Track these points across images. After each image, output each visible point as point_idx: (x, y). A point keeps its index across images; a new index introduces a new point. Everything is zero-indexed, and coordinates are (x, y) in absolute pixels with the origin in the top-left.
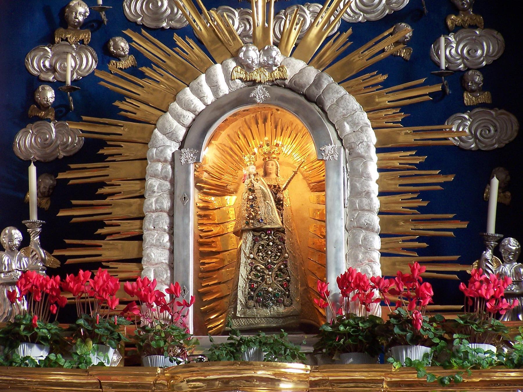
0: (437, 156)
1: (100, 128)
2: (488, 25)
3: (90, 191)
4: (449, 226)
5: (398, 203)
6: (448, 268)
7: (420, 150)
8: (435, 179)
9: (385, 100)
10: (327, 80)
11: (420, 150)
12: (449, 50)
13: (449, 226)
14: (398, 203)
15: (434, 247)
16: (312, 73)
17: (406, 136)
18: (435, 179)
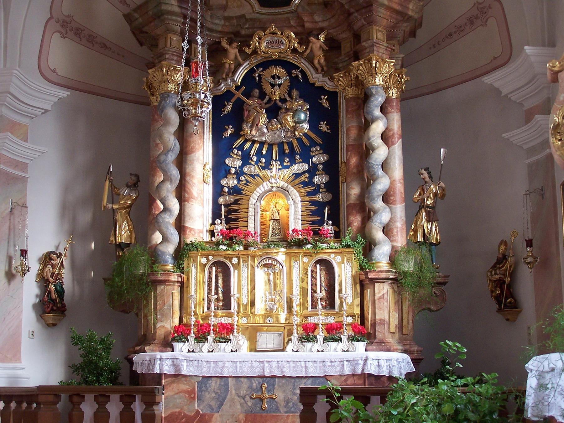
0: (314, 203)
2: (326, 174)
3: (236, 211)
4: (316, 218)
5: (305, 213)
6: (316, 228)
7: (310, 202)
8: (313, 208)
9: (302, 191)
10: (290, 186)
11: (310, 202)
12: (317, 180)
13: (316, 218)
14: (305, 213)
15: (313, 223)
16: (286, 184)
17: (307, 199)
18: (313, 208)
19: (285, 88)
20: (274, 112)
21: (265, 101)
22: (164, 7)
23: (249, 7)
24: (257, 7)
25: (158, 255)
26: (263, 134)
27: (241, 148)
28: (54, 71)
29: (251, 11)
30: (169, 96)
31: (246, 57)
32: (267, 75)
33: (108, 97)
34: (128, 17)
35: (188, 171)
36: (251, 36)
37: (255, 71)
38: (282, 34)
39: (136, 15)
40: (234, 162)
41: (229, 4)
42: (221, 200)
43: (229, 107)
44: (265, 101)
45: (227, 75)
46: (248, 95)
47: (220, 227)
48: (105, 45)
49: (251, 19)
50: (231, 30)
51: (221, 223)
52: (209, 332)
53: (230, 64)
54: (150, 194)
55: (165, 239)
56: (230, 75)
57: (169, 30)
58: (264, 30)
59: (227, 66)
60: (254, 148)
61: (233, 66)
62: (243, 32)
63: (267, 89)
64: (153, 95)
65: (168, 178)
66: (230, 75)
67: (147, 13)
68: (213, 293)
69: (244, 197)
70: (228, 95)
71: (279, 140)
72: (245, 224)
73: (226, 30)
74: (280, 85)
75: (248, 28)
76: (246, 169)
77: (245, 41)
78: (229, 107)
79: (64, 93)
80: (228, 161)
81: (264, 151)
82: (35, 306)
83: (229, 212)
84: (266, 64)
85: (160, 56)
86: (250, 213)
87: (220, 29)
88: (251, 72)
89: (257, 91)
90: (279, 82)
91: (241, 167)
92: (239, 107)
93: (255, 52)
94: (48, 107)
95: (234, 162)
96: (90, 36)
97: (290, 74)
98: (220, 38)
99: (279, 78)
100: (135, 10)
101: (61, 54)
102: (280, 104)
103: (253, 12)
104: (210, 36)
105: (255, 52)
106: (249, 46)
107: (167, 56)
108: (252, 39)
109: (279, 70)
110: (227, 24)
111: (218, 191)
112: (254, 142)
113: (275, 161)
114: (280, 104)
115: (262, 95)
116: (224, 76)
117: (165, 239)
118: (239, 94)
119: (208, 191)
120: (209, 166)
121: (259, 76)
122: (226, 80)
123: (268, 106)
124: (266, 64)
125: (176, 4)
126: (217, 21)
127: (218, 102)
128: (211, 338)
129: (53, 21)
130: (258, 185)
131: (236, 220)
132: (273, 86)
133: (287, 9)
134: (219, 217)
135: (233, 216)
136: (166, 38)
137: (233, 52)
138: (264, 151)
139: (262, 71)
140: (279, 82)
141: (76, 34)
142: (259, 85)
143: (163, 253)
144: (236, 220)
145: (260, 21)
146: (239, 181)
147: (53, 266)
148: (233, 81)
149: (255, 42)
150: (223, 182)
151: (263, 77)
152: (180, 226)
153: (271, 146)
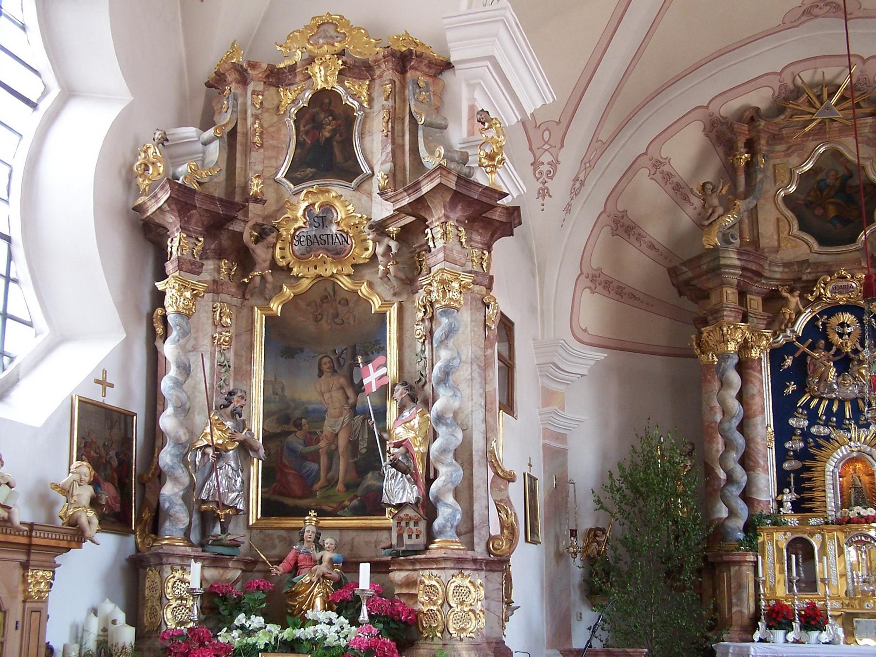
1: (808, 463)
16: (869, 449)
19: (855, 337)
20: (845, 363)
21: (832, 352)
22: (723, 262)
23: (806, 246)
24: (816, 246)
25: (728, 532)
26: (833, 390)
27: (806, 406)
28: (585, 331)
29: (809, 251)
30: (729, 357)
31: (807, 304)
32: (834, 321)
33: (635, 351)
34: (673, 272)
35: (751, 436)
36: (815, 282)
37: (818, 319)
38: (852, 277)
39: (684, 269)
40: (799, 422)
41: (782, 245)
42: (786, 465)
43: (789, 362)
44: (832, 352)
45: (786, 326)
46: (812, 347)
47: (788, 497)
48: (634, 296)
49: (814, 264)
50: (791, 277)
51: (790, 492)
52: (794, 620)
53: (790, 314)
54: (706, 464)
55: (732, 513)
56: (790, 325)
57: (723, 284)
58: (831, 274)
59: (788, 317)
60: (822, 406)
61: (794, 317)
62: (805, 278)
63: (835, 338)
64: (703, 353)
65: (728, 444)
66: (790, 325)
67: (700, 266)
68: (794, 574)
69: (819, 464)
70: (789, 348)
71: (853, 396)
72: (822, 494)
73: (785, 277)
74: (849, 334)
75: (809, 273)
76: (814, 430)
77: (807, 287)
78: (789, 362)
79: (601, 355)
80: (792, 422)
81: (835, 408)
82: (580, 585)
83: (799, 481)
84: (834, 310)
85: (716, 313)
86: (827, 482)
87: (778, 276)
88: (814, 319)
89: (823, 342)
90: (849, 330)
91: (809, 427)
92: (801, 362)
93: (819, 298)
94: (585, 372)
95: (799, 422)
96: (619, 287)
97: (861, 321)
98: (777, 286)
99: (848, 326)
100: (684, 264)
101: (593, 311)
102: (852, 356)
103: (811, 252)
104: (767, 284)
105: (819, 298)
106: (812, 292)
107: (725, 313)
108: (815, 285)
109: (847, 317)
110: (786, 270)
111: (782, 455)
112: (821, 399)
113: (848, 420)
114: (852, 356)
115: (829, 345)
116: (783, 327)
117: (732, 513)
118: (803, 348)
119: (772, 454)
120: (771, 429)
121: (823, 324)
122: (785, 331)
123: (837, 358)
124: (834, 310)
125: (736, 257)
126: (776, 269)
127: (776, 355)
128: (796, 625)
129: (583, 277)
130: (836, 449)
131: (810, 489)
132: (841, 335)
133: (852, 247)
134: (788, 486)
135: (807, 485)
136: (721, 293)
137: (794, 300)
138: (835, 408)
139: (827, 319)
140: (849, 330)
141: (604, 287)
142: (824, 335)
143: (733, 530)
144: (810, 489)
145: (824, 264)
146: (806, 443)
147: (599, 543)
148: (793, 332)
149: (819, 289)
150: (788, 445)
151: (828, 325)
152: (746, 496)
153: (842, 403)
